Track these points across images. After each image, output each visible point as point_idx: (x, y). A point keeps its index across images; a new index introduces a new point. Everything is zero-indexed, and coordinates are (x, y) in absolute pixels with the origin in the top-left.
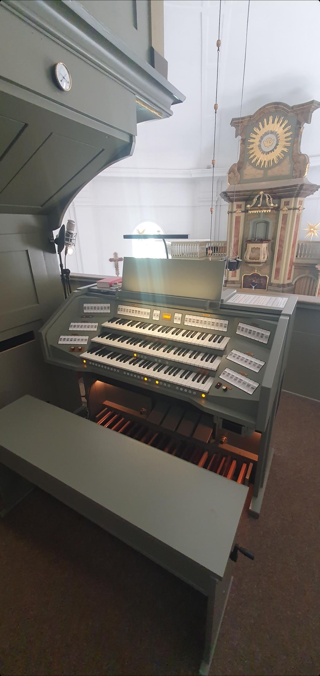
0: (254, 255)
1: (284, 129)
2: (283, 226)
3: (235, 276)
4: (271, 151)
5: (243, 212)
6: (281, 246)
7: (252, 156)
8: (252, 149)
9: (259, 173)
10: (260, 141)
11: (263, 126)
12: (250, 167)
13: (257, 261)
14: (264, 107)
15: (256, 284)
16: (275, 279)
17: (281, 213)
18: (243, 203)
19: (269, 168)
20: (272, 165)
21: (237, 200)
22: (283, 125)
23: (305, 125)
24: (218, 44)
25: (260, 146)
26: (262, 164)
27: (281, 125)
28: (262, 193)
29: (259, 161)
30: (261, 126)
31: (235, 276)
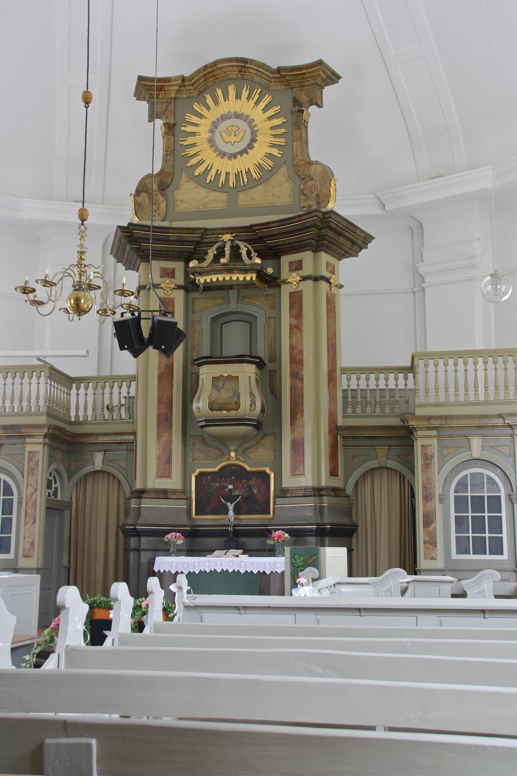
0: (224, 395)
1: (265, 110)
2: (294, 322)
3: (169, 476)
4: (241, 153)
5: (179, 287)
6: (296, 376)
7: (193, 161)
8: (194, 145)
9: (218, 200)
10: (212, 131)
11: (216, 102)
12: (191, 185)
13: (232, 414)
14: (215, 64)
15: (237, 496)
16: (293, 474)
17: (285, 291)
18: (178, 266)
19: (240, 188)
20: (245, 183)
21: (160, 255)
22: (262, 105)
23: (313, 109)
24: (87, 100)
25: (211, 141)
26: (223, 178)
27: (257, 103)
28: (227, 237)
29: (213, 173)
30: (209, 100)
31: (169, 476)
